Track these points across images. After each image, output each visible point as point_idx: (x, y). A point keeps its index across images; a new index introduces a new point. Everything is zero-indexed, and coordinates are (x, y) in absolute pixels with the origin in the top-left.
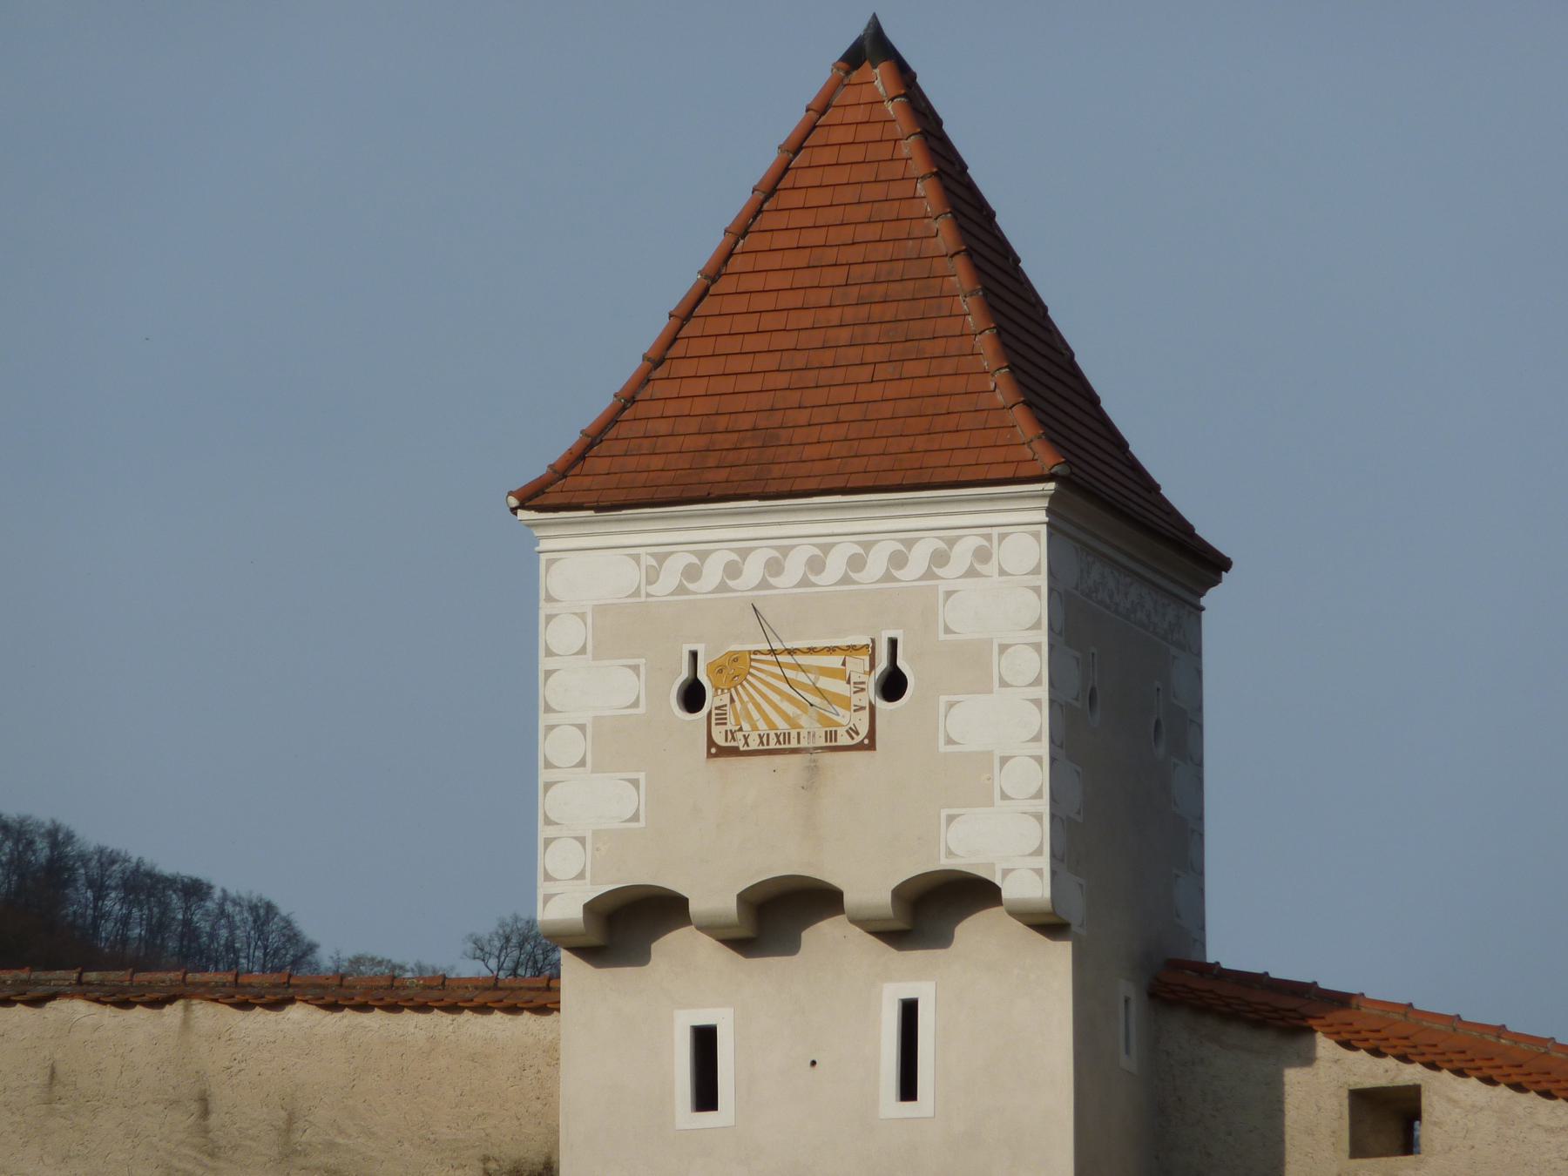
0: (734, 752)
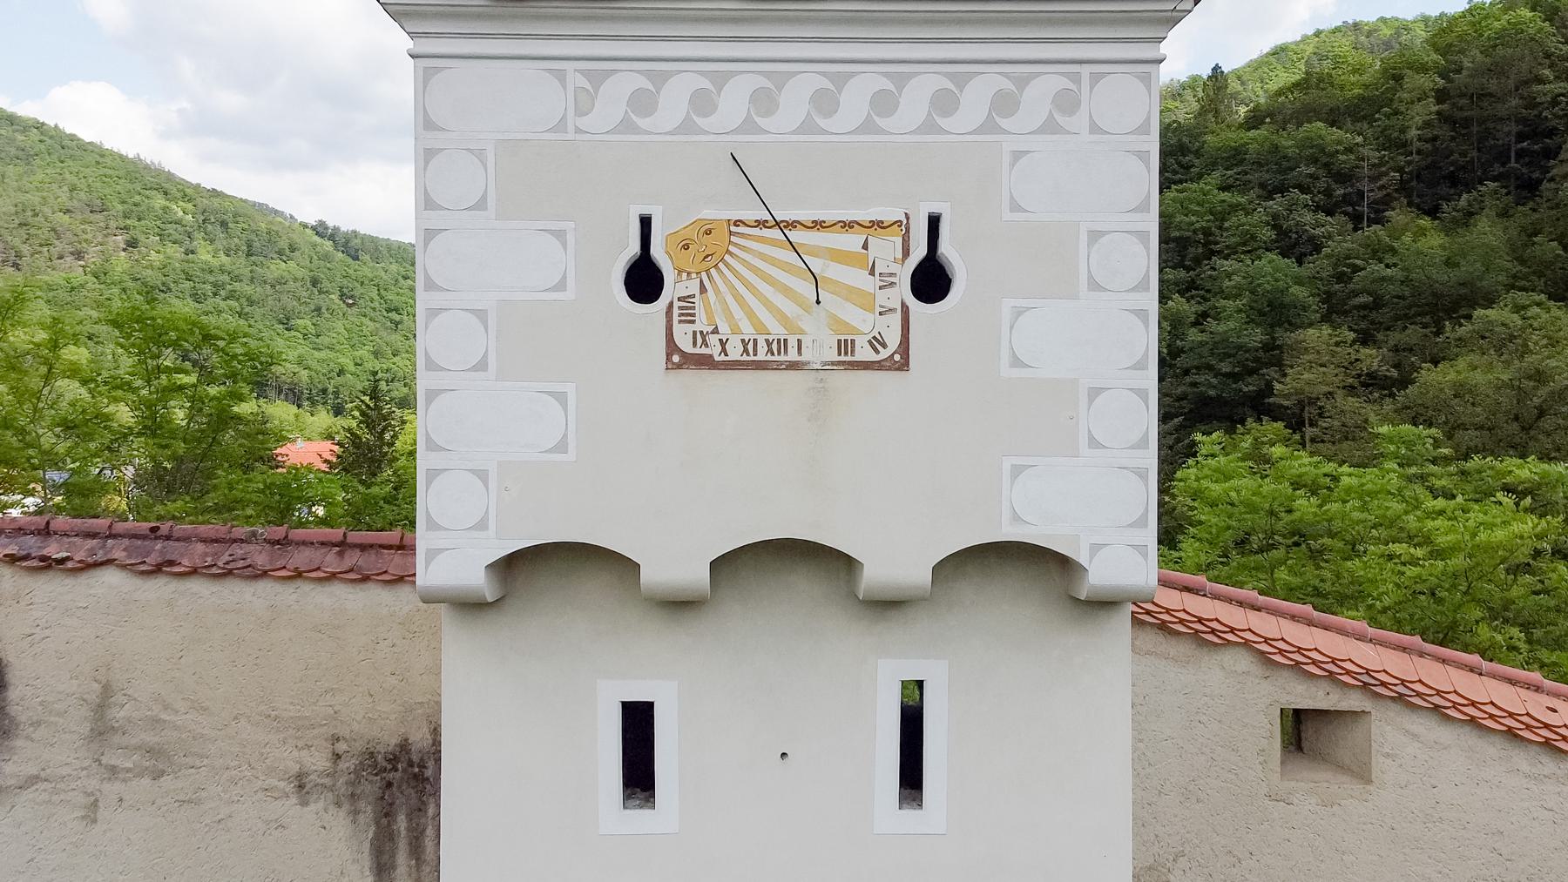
0: (705, 362)
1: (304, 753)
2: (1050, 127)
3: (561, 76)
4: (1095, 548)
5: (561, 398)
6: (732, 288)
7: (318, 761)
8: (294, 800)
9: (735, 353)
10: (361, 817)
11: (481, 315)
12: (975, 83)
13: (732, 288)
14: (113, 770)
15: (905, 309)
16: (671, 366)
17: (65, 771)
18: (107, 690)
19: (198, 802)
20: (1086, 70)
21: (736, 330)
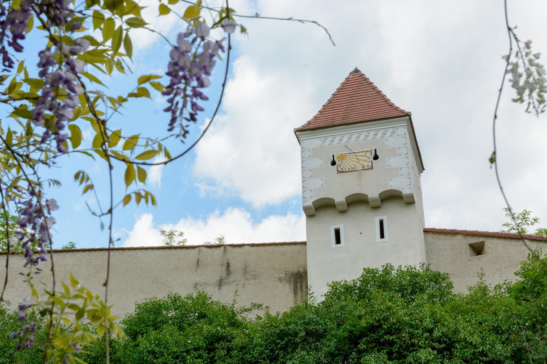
0: (343, 172)
1: (280, 274)
2: (391, 136)
3: (321, 140)
4: (403, 189)
5: (322, 179)
6: (346, 162)
7: (283, 275)
8: (279, 282)
9: (347, 170)
10: (291, 284)
11: (310, 170)
12: (379, 132)
13: (346, 162)
14: (247, 279)
15: (372, 161)
16: (338, 173)
17: (240, 279)
18: (246, 266)
19: (262, 283)
20: (396, 128)
21: (347, 167)
